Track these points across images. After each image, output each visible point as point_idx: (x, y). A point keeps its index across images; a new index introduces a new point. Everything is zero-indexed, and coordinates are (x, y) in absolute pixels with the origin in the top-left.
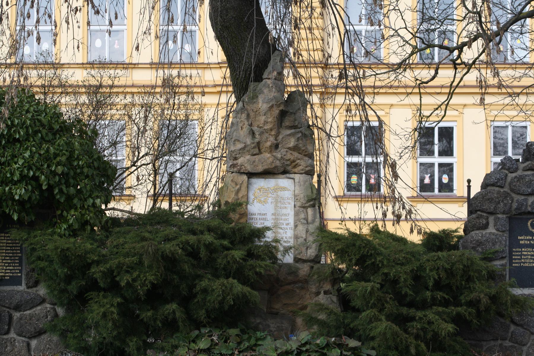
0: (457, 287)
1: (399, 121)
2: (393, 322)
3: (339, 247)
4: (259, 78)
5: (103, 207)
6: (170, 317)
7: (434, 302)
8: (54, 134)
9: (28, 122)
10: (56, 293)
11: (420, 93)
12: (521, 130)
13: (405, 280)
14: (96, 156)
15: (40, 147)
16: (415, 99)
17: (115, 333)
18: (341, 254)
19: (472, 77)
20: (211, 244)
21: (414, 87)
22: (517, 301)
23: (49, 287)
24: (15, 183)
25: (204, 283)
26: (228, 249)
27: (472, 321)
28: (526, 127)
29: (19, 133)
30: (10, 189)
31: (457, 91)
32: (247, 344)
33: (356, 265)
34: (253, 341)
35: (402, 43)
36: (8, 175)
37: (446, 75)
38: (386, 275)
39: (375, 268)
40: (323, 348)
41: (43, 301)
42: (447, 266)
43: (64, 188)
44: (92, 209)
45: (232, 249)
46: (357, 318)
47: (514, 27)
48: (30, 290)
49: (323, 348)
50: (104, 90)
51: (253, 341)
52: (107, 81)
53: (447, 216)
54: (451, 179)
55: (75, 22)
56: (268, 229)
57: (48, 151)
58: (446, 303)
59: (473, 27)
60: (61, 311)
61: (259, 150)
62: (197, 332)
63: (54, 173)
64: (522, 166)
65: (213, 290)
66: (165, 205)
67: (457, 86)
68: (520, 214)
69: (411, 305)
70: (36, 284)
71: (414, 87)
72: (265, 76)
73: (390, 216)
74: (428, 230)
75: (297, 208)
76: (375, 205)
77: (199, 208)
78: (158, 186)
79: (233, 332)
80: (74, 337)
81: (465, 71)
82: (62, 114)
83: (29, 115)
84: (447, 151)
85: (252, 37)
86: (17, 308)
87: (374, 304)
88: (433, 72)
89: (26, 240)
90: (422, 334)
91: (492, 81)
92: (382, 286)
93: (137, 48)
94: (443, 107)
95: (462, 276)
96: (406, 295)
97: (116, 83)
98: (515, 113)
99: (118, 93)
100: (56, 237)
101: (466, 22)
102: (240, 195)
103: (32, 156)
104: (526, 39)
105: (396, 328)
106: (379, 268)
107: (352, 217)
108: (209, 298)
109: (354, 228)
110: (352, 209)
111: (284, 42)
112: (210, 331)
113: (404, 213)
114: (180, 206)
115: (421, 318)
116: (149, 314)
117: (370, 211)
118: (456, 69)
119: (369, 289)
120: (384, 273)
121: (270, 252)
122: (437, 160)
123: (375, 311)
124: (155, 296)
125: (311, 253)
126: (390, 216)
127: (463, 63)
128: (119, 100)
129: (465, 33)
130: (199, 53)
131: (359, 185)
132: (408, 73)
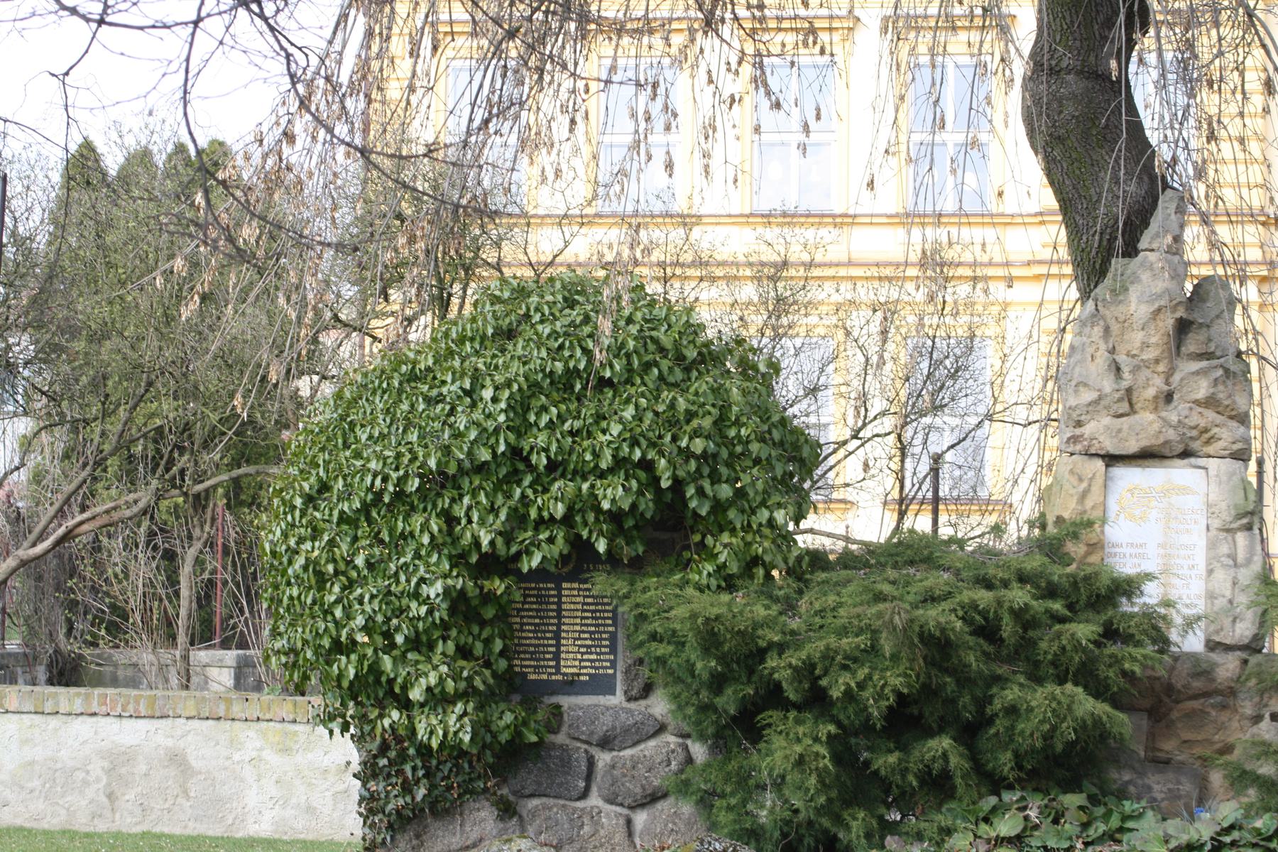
8: (687, 370)
15: (657, 398)
23: (675, 697)
24: (602, 475)
30: (592, 486)
34: (1115, 822)
44: (766, 531)
45: (1070, 620)
48: (632, 705)
49: (1269, 839)
50: (792, 272)
52: (797, 254)
55: (729, 126)
56: (1149, 577)
57: (672, 406)
60: (699, 751)
63: (687, 454)
66: (922, 524)
70: (647, 690)
77: (997, 530)
79: (1072, 800)
80: (730, 808)
83: (634, 329)
89: (626, 596)
93: (871, 184)
100: (690, 591)
102: (1089, 503)
103: (639, 418)
112: (1023, 798)
114: (955, 526)
116: (892, 759)
121: (1154, 629)
124: (905, 720)
130: (1000, 194)
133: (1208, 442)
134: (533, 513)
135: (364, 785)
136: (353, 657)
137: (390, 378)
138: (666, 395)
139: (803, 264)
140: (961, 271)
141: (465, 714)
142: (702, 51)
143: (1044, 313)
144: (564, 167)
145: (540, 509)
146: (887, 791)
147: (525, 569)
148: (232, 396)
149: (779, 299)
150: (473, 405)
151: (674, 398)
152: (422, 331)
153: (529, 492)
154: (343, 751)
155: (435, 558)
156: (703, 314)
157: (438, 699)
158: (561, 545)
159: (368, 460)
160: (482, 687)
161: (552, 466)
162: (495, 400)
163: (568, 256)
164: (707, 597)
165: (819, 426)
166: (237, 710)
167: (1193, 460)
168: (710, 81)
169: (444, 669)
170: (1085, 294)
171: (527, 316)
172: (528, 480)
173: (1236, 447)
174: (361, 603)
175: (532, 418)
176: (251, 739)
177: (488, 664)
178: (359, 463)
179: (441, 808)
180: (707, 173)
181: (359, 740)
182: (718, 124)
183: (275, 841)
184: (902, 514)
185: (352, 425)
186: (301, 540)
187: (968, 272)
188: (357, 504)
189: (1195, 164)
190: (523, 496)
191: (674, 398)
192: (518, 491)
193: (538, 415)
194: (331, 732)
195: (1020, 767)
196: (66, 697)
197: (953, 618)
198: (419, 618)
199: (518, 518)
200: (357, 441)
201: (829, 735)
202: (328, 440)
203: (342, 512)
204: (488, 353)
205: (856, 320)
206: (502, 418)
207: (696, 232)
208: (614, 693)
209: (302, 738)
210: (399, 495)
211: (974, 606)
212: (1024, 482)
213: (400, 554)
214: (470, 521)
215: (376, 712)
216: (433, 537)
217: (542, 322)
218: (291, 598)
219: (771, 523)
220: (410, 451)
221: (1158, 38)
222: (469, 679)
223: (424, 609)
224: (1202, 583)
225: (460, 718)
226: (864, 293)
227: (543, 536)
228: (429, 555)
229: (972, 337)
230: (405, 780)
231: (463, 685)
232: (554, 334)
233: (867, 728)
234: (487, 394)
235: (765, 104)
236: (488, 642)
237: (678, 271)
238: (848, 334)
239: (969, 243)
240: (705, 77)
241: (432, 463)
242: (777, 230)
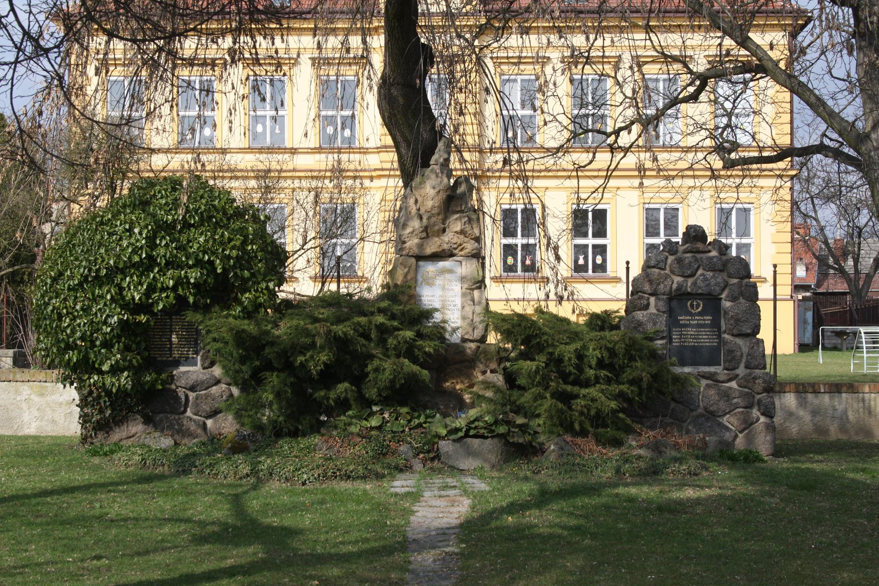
0: (620, 366)
1: (556, 201)
2: (557, 399)
3: (506, 327)
4: (426, 164)
5: (277, 289)
6: (343, 396)
7: (597, 380)
8: (228, 219)
9: (203, 207)
10: (231, 373)
11: (578, 177)
12: (672, 212)
13: (570, 359)
14: (269, 241)
15: (215, 232)
16: (574, 182)
17: (289, 412)
18: (507, 334)
19: (630, 160)
20: (382, 324)
21: (573, 171)
22: (677, 379)
23: (224, 367)
24: (190, 267)
25: (376, 362)
26: (399, 329)
27: (634, 398)
28: (677, 209)
29: (194, 218)
30: (186, 272)
31: (614, 174)
32: (417, 421)
33: (522, 344)
34: (422, 419)
35: (560, 128)
36: (184, 259)
37: (603, 158)
38: (551, 354)
39: (540, 348)
40: (491, 425)
41: (218, 382)
42: (610, 346)
43: (238, 271)
44: (265, 292)
45: (402, 330)
46: (523, 395)
47: (669, 112)
48: (205, 371)
49: (491, 425)
50: (272, 174)
51: (422, 419)
52: (275, 166)
53: (607, 296)
54: (604, 261)
55: (242, 108)
56: (437, 310)
57: (222, 235)
58: (609, 381)
59: (630, 113)
60: (235, 391)
61: (427, 234)
62: (369, 411)
63: (229, 257)
64: (681, 249)
65: (384, 369)
66: (333, 287)
67: (614, 170)
68: (680, 295)
69: (574, 383)
70: (212, 364)
71: (573, 171)
72: (432, 162)
73: (552, 296)
74: (589, 311)
75: (464, 290)
76: (538, 285)
77: (369, 289)
78: (326, 269)
79: (404, 410)
80: (249, 416)
81: (622, 154)
82: (234, 200)
83: (204, 201)
84: (601, 232)
85: (419, 124)
86: (192, 389)
87: (539, 382)
88: (591, 155)
89: (202, 322)
90: (586, 411)
91: (648, 164)
92: (547, 365)
93: (306, 135)
94: (601, 190)
95: (624, 355)
96: (570, 373)
97: (284, 168)
98: (670, 195)
99: (286, 178)
100: (231, 319)
101: (621, 108)
102: (409, 277)
103: (206, 241)
104: (681, 123)
105: (560, 405)
106: (544, 348)
107: (516, 297)
108: (380, 377)
109: (519, 309)
110: (516, 290)
111: (450, 128)
112: (381, 409)
113: (566, 294)
114: (347, 288)
115: (584, 396)
116: (322, 393)
117: (533, 291)
118: (613, 153)
119: (534, 368)
120: (548, 353)
121: (439, 333)
122: (590, 241)
123: (540, 389)
124: (329, 377)
125: (478, 334)
126: (552, 296)
127: (620, 147)
128: (283, 184)
129: (621, 119)
130: (367, 140)
131: (515, 265)
132: (568, 157)
133: (461, 250)
134: (159, 285)
135: (82, 410)
136: (76, 352)
137: (91, 224)
138: (220, 231)
139: (277, 171)
140: (348, 174)
141: (128, 376)
142: (229, 74)
143: (388, 192)
144: (167, 127)
145: (162, 283)
146: (320, 407)
147: (156, 311)
148: (14, 232)
149: (267, 187)
150: (130, 236)
151: (223, 233)
152: (102, 203)
153: (157, 275)
154: (71, 393)
155: (114, 305)
156: (235, 194)
157: (115, 370)
158: (172, 299)
159: (82, 261)
160: (136, 364)
161: (168, 263)
162: (140, 233)
163: (170, 167)
164: (238, 322)
165: (284, 244)
166: (19, 376)
167: (455, 258)
168: (233, 88)
169: (119, 356)
170: (406, 185)
171: (155, 195)
172: (156, 270)
173: (475, 251)
174: (79, 326)
175: (158, 242)
176: (26, 390)
177: (138, 354)
178: (77, 263)
179: (118, 420)
180: (231, 131)
181: (78, 389)
182: (237, 108)
183: (39, 436)
184: (323, 285)
185: (74, 245)
186: (51, 299)
187: (351, 174)
188: (76, 282)
189: (454, 125)
190: (154, 277)
191: (223, 233)
192: (152, 275)
193: (161, 241)
194: (65, 386)
195: (380, 395)
196: (836, 380)
197: (349, 329)
198: (107, 333)
199: (151, 289)
200: (77, 253)
201: (291, 383)
202: (63, 252)
203: (69, 285)
204: (137, 212)
205: (301, 196)
206: (144, 242)
207: (228, 157)
208: (196, 365)
209: (50, 389)
210: (97, 277)
211: (359, 324)
212: (379, 269)
213: (97, 304)
214: (130, 289)
215: (87, 376)
216: (112, 296)
217: (162, 198)
218: (46, 325)
219: (267, 288)
220: (102, 257)
221: (438, 68)
222: (131, 361)
223: (109, 329)
224: (459, 313)
225: (126, 378)
226: (305, 184)
227: (164, 295)
228: (111, 304)
229: (354, 203)
230: (101, 407)
231: (127, 364)
232: (167, 204)
233: (311, 379)
234: (136, 230)
235: (258, 99)
236: (138, 344)
237: (221, 174)
238: (298, 202)
239: (351, 161)
240: (231, 86)
241: (112, 262)
242: (265, 155)
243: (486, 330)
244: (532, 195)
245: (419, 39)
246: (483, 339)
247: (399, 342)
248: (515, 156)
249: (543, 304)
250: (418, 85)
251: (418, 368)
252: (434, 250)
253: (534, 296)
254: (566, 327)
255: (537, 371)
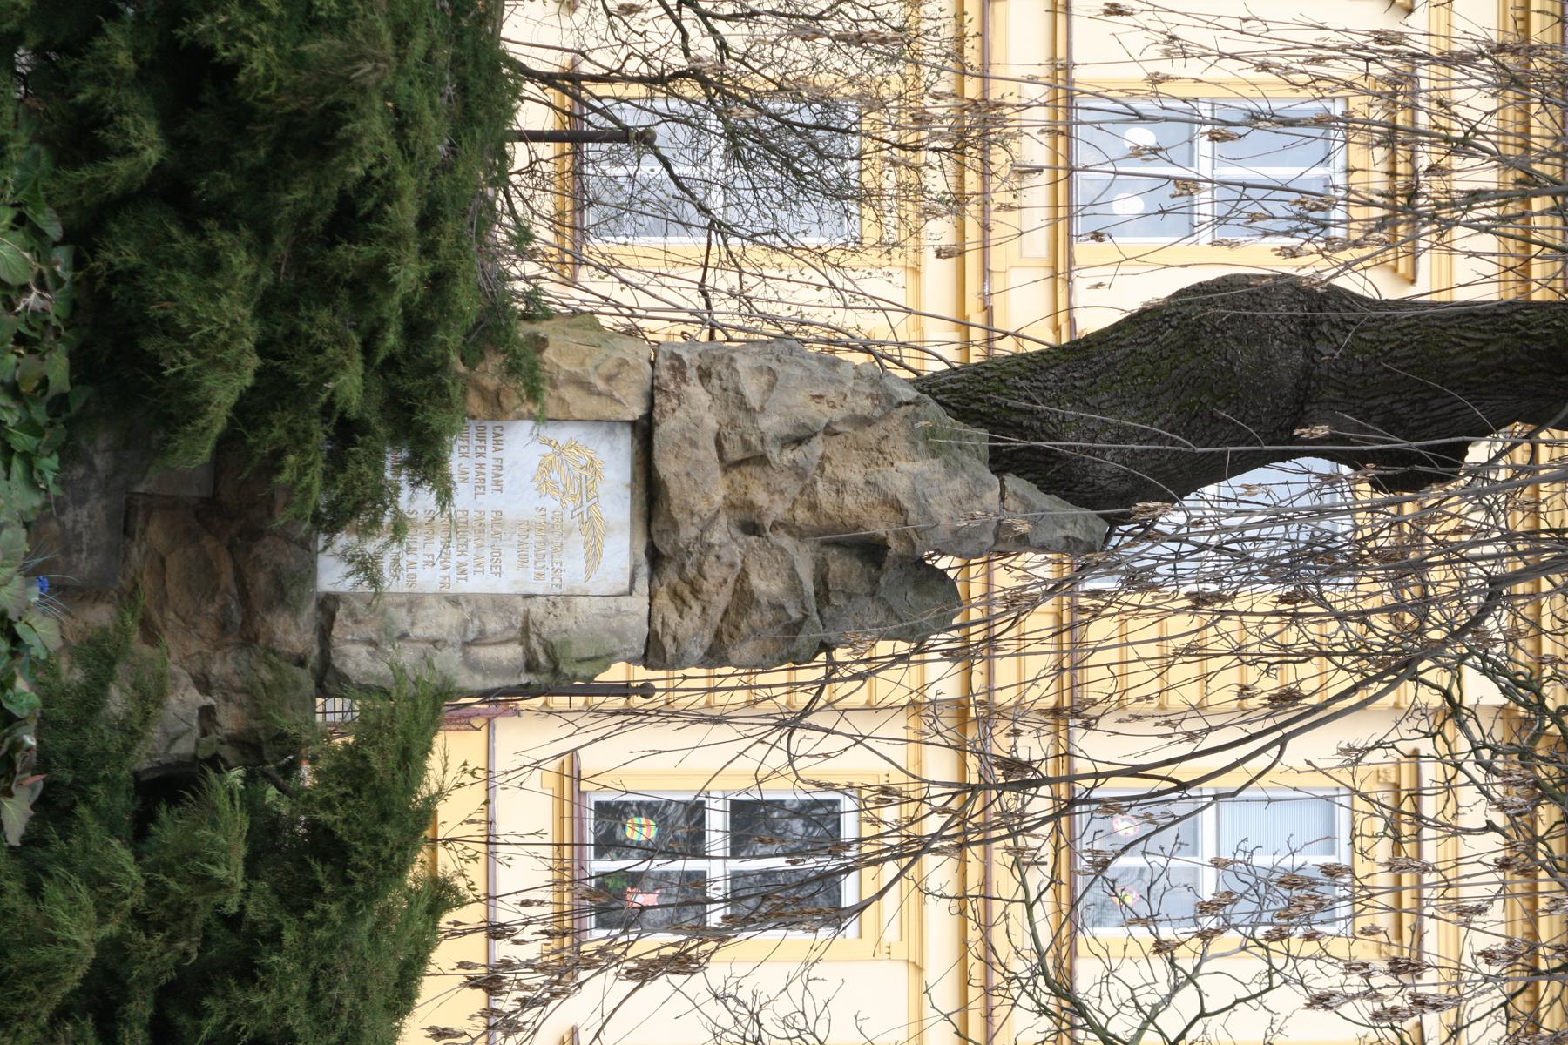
3: (376, 762)
13: (254, 1010)
18: (353, 773)
20: (388, 286)
35: (1146, 1000)
38: (275, 938)
56: (445, 497)
61: (738, 464)
62: (54, 231)
65: (214, 295)
75: (522, 606)
79: (57, 368)
87: (164, 892)
92: (233, 922)
96: (200, 1013)
102: (569, 393)
105: (72, 979)
106: (298, 911)
109: (451, 816)
110: (529, 811)
112: (59, 282)
113: (506, 1003)
116: (123, 59)
117: (525, 876)
119: (220, 872)
121: (359, 506)
123: (136, 896)
125: (356, 659)
143: (896, 317)
170: (926, 385)
195: (113, 279)
197: (370, 160)
211: (391, 196)
224: (434, 587)
243: (366, 690)
244: (891, 869)
245: (1483, 432)
246: (329, 679)
247: (320, 351)
248: (1041, 804)
249: (471, 914)
250: (1305, 433)
251: (219, 428)
252: (673, 487)
253: (506, 880)
254: (377, 999)
255: (205, 882)
